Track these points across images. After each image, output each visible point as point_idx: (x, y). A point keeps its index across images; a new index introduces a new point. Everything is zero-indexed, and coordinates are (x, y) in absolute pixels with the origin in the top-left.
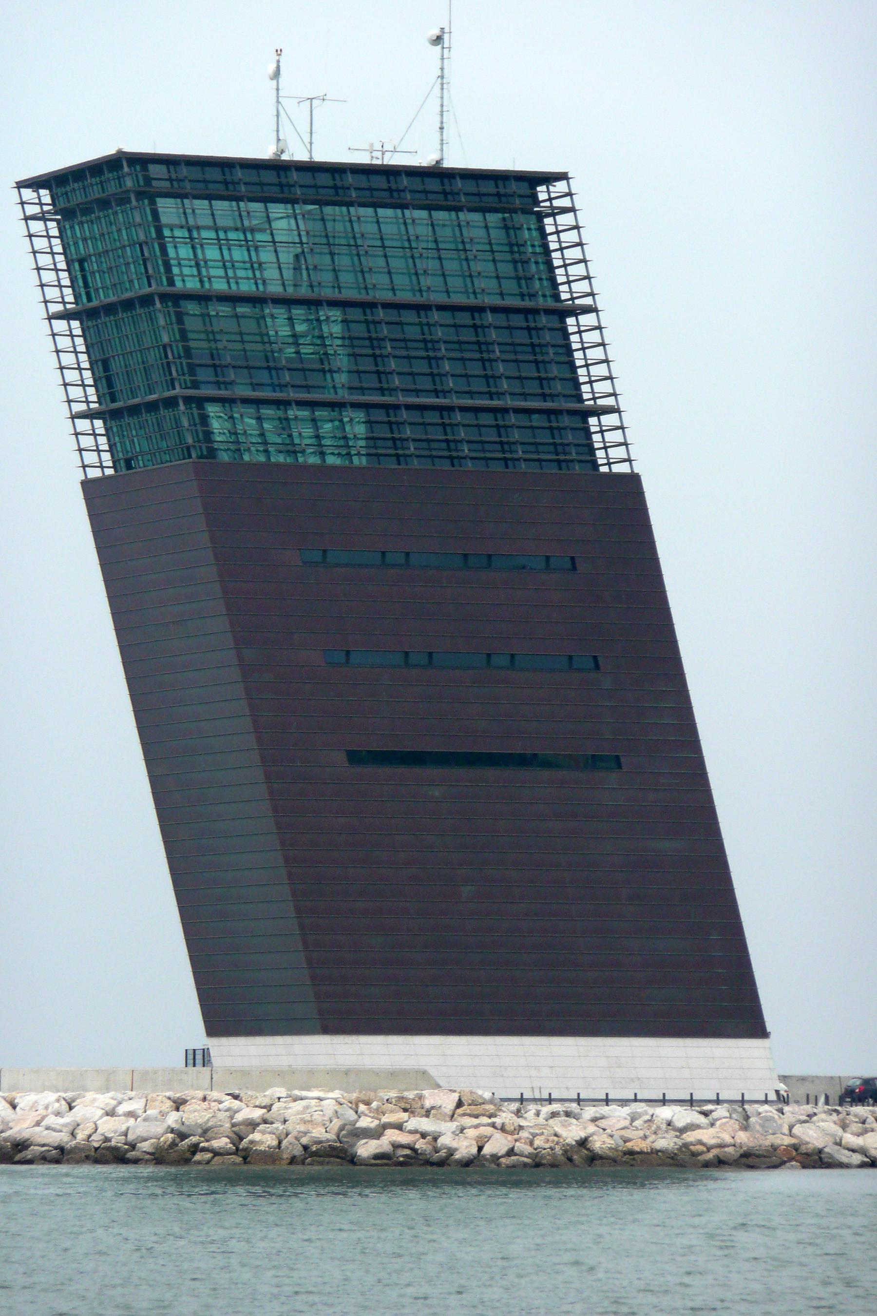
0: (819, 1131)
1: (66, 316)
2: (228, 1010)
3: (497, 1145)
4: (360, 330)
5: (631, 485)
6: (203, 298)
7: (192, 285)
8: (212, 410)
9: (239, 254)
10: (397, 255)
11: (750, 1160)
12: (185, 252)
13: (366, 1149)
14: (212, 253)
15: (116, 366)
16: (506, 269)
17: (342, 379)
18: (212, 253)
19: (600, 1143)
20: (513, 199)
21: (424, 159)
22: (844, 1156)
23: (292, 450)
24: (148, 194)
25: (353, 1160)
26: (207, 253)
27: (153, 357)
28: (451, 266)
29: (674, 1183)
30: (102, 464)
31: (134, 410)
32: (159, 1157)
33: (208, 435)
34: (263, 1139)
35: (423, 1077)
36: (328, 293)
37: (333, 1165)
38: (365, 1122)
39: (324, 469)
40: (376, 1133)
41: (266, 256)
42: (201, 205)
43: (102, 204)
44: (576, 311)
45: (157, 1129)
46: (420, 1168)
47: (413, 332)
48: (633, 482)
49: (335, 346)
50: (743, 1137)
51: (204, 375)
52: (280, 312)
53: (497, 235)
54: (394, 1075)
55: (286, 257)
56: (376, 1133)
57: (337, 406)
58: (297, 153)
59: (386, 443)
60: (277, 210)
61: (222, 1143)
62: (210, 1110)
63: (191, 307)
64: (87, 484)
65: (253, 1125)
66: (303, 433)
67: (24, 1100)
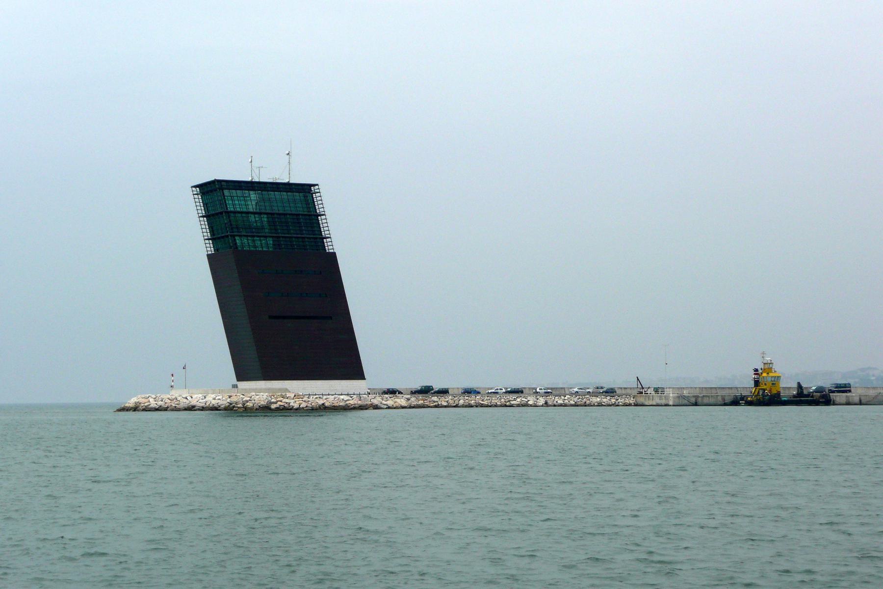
0: (377, 401)
1: (203, 217)
2: (242, 374)
3: (303, 405)
4: (270, 219)
5: (334, 255)
6: (235, 212)
7: (232, 209)
8: (237, 238)
9: (243, 202)
10: (280, 203)
11: (362, 408)
12: (230, 202)
13: (273, 406)
14: (237, 202)
15: (215, 228)
16: (305, 206)
17: (267, 231)
18: (237, 202)
19: (327, 404)
20: (306, 190)
21: (286, 181)
22: (383, 406)
23: (255, 247)
24: (222, 189)
25: (270, 409)
26: (234, 202)
27: (223, 226)
28: (292, 205)
29: (863, 370)
30: (211, 250)
31: (219, 238)
32: (226, 409)
33: (236, 244)
34: (250, 404)
35: (287, 390)
36: (263, 211)
37: (266, 410)
38: (273, 400)
39: (263, 251)
40: (276, 403)
41: (249, 203)
42: (234, 191)
43: (213, 193)
44: (321, 215)
45: (225, 402)
46: (286, 411)
47: (283, 220)
48: (334, 254)
49: (266, 224)
50: (359, 402)
51: (235, 230)
52: (252, 216)
53: (302, 198)
54: (280, 390)
55: (254, 203)
56: (276, 403)
57: (266, 237)
58: (257, 180)
59: (277, 245)
60: (251, 192)
61: (240, 405)
62: (237, 398)
63: (232, 215)
64: (208, 255)
65: (247, 401)
66: (258, 243)
67: (194, 396)
